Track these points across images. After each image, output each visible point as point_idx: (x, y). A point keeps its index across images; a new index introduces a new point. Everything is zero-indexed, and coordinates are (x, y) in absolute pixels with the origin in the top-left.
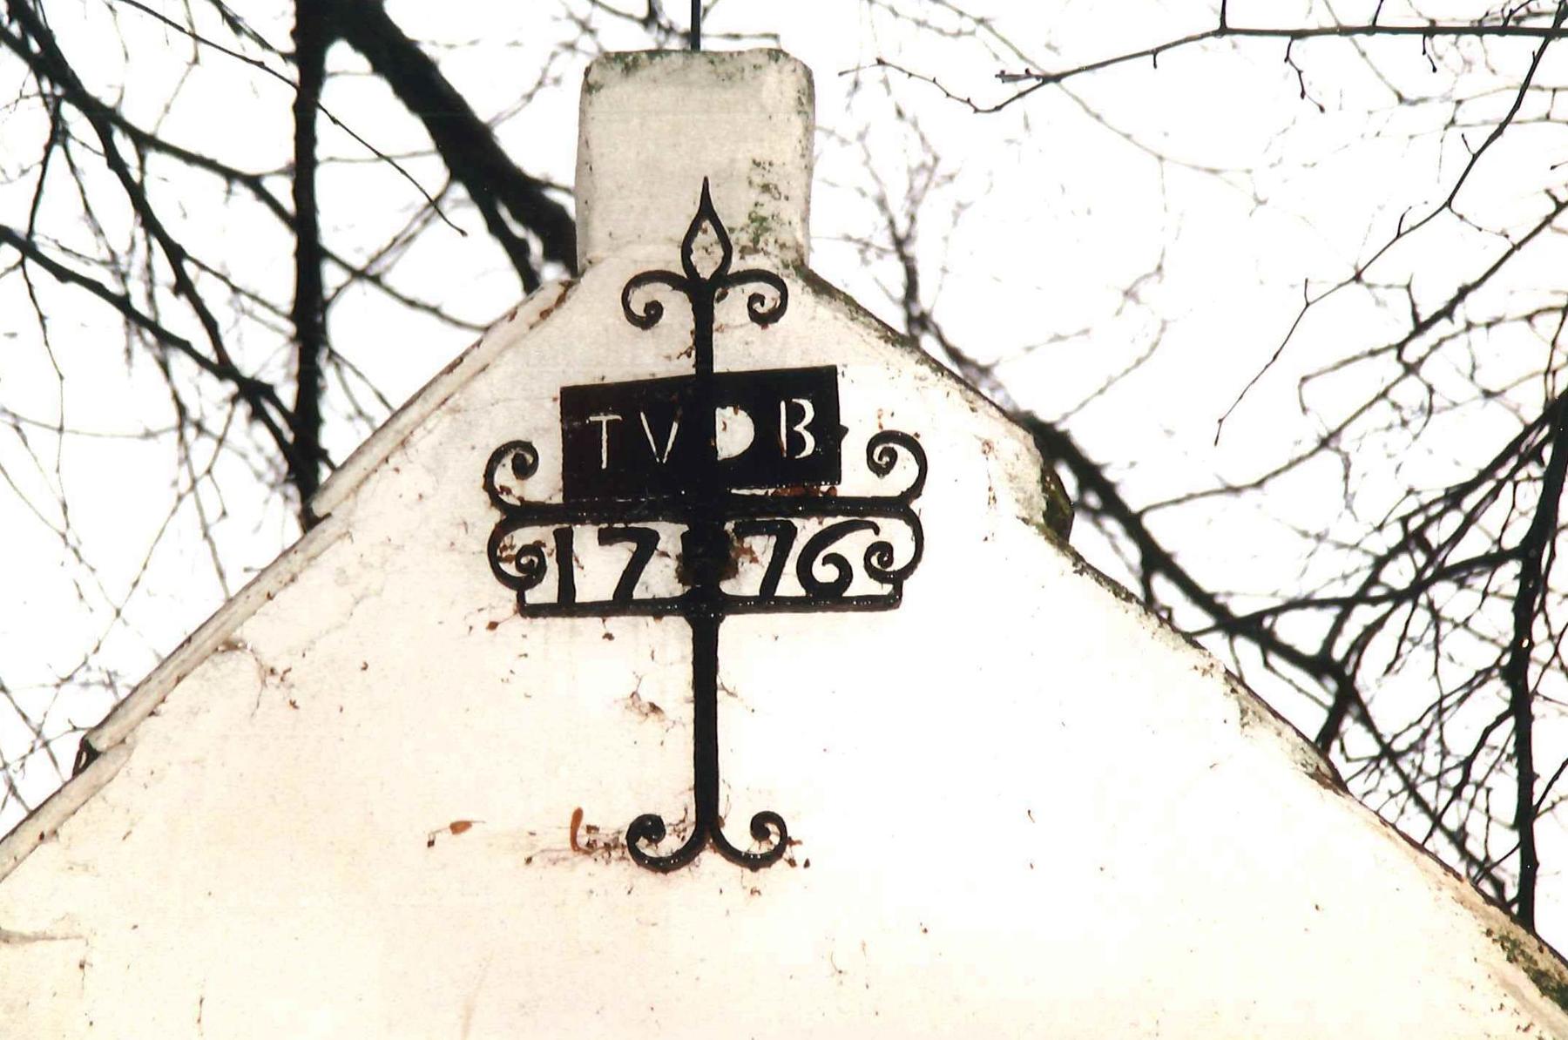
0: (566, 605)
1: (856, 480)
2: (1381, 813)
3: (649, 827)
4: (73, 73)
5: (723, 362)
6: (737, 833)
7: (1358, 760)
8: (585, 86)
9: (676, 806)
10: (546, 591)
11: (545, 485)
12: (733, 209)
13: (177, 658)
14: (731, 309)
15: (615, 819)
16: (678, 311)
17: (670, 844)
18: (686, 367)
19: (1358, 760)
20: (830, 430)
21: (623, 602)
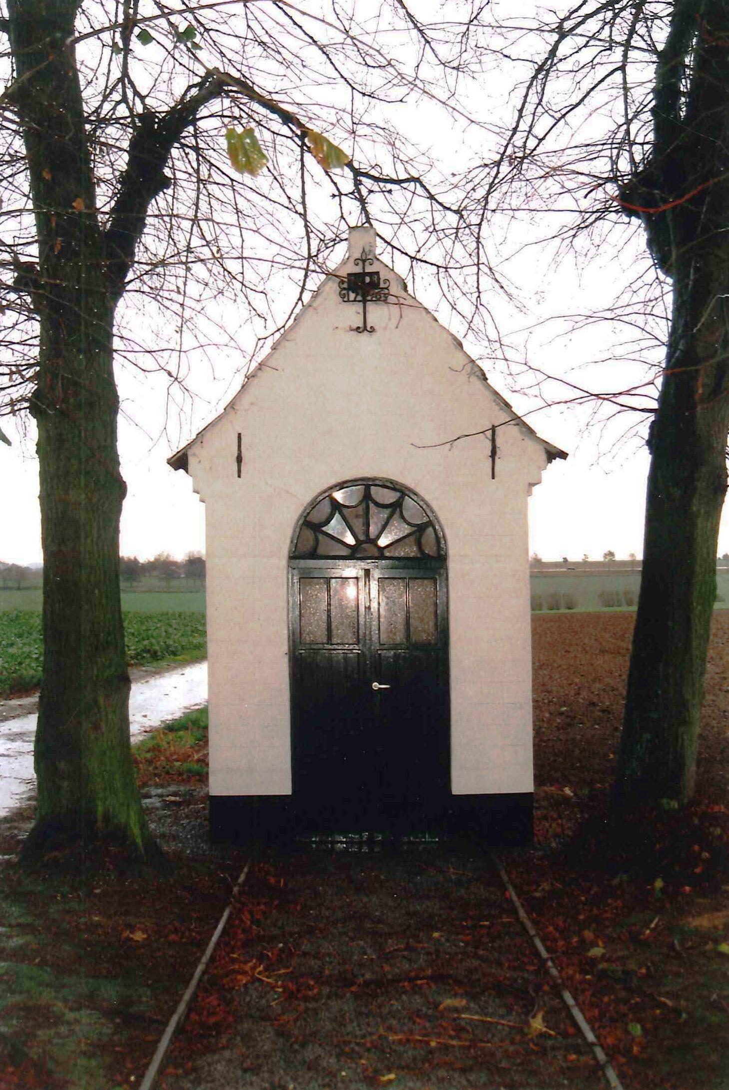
0: (348, 301)
1: (382, 285)
2: (620, 124)
3: (358, 328)
4: (723, 502)
5: (366, 271)
6: (368, 329)
7: (657, 274)
8: (553, 451)
9: (361, 325)
10: (345, 299)
11: (345, 285)
12: (367, 250)
13: (707, 308)
14: (367, 263)
15: (355, 326)
16: (360, 263)
17: (361, 330)
18: (362, 271)
19: (657, 274)
20: (379, 279)
21: (355, 301)
